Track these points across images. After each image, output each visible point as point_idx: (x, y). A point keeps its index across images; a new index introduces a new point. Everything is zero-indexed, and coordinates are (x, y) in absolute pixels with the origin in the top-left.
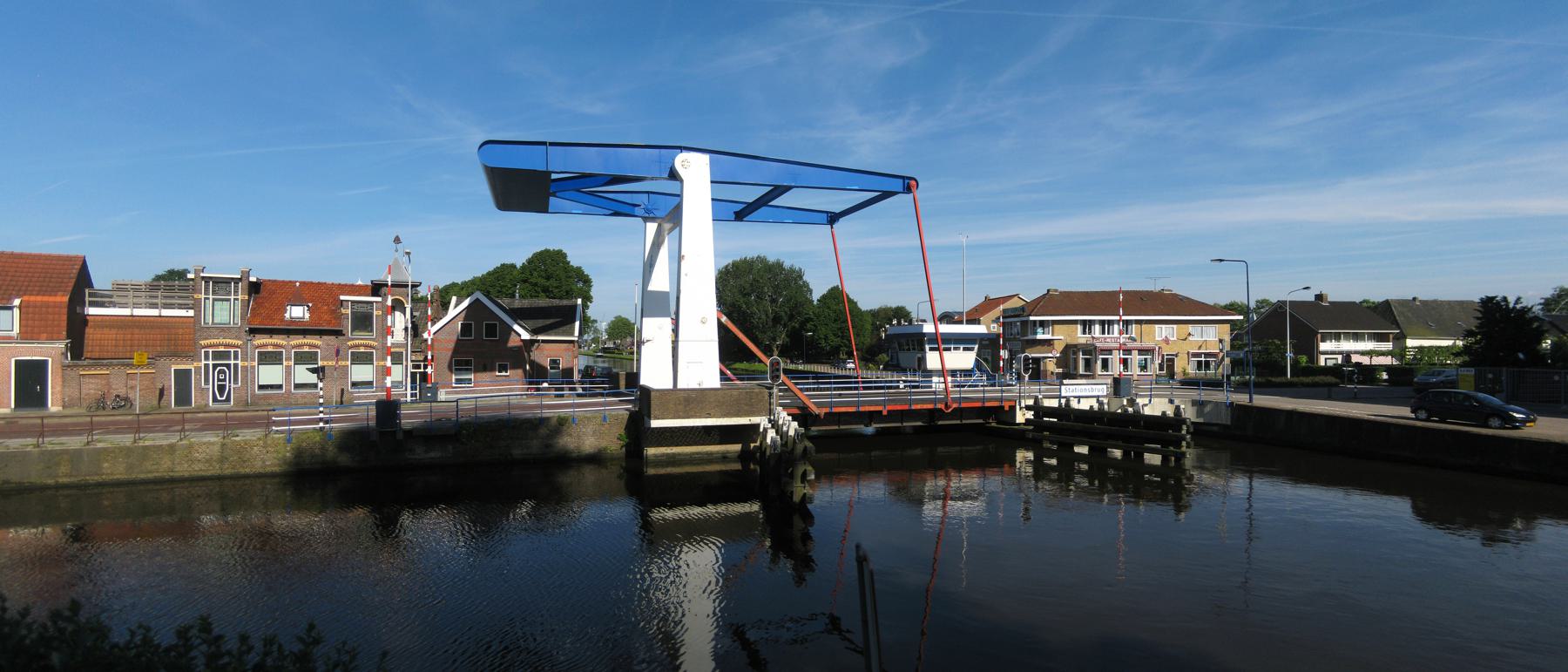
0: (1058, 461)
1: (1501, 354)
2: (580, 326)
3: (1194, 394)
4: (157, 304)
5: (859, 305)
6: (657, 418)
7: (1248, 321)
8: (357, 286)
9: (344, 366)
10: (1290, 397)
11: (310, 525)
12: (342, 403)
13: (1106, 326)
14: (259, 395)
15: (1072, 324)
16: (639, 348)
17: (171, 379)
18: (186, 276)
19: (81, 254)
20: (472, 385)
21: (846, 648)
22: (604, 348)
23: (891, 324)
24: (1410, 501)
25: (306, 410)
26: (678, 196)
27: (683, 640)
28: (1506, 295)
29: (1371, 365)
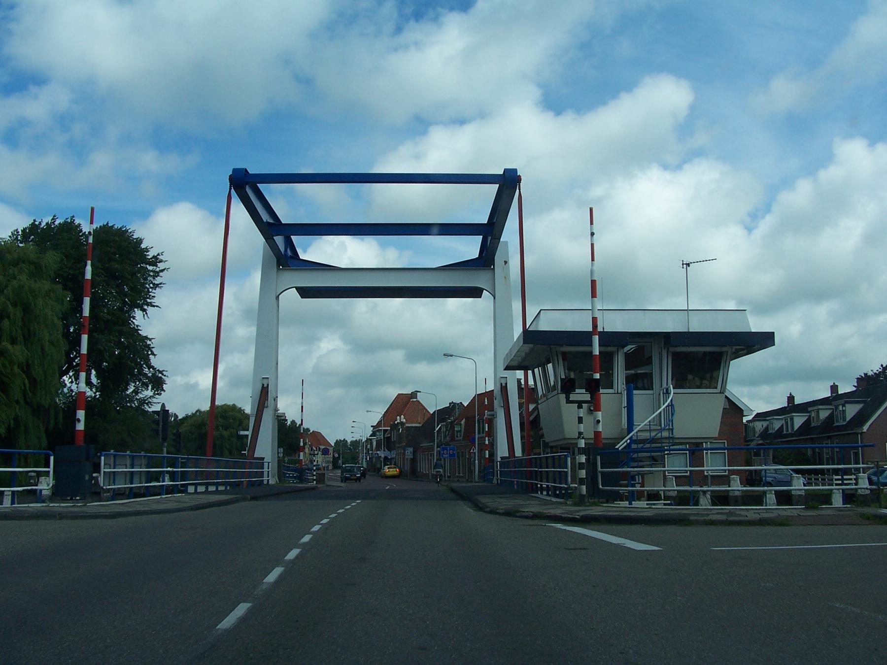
0: (36, 225)
1: (122, 340)
2: (768, 417)
3: (497, 393)
4: (480, 434)
5: (202, 410)
6: (104, 458)
7: (137, 337)
8: (92, 268)
9: (162, 450)
10: (88, 348)
11: (79, 420)
12: (688, 265)
13: (402, 466)
14: (725, 440)
15: (93, 213)
16: (804, 408)
17: (868, 543)
18: (807, 409)
19: (244, 167)
20: (448, 474)
21: (303, 380)
22: (673, 442)
23: (542, 493)
24: (517, 365)
25: (623, 398)
26: (789, 482)
27: (162, 287)
28: (294, 419)
29: (603, 332)
